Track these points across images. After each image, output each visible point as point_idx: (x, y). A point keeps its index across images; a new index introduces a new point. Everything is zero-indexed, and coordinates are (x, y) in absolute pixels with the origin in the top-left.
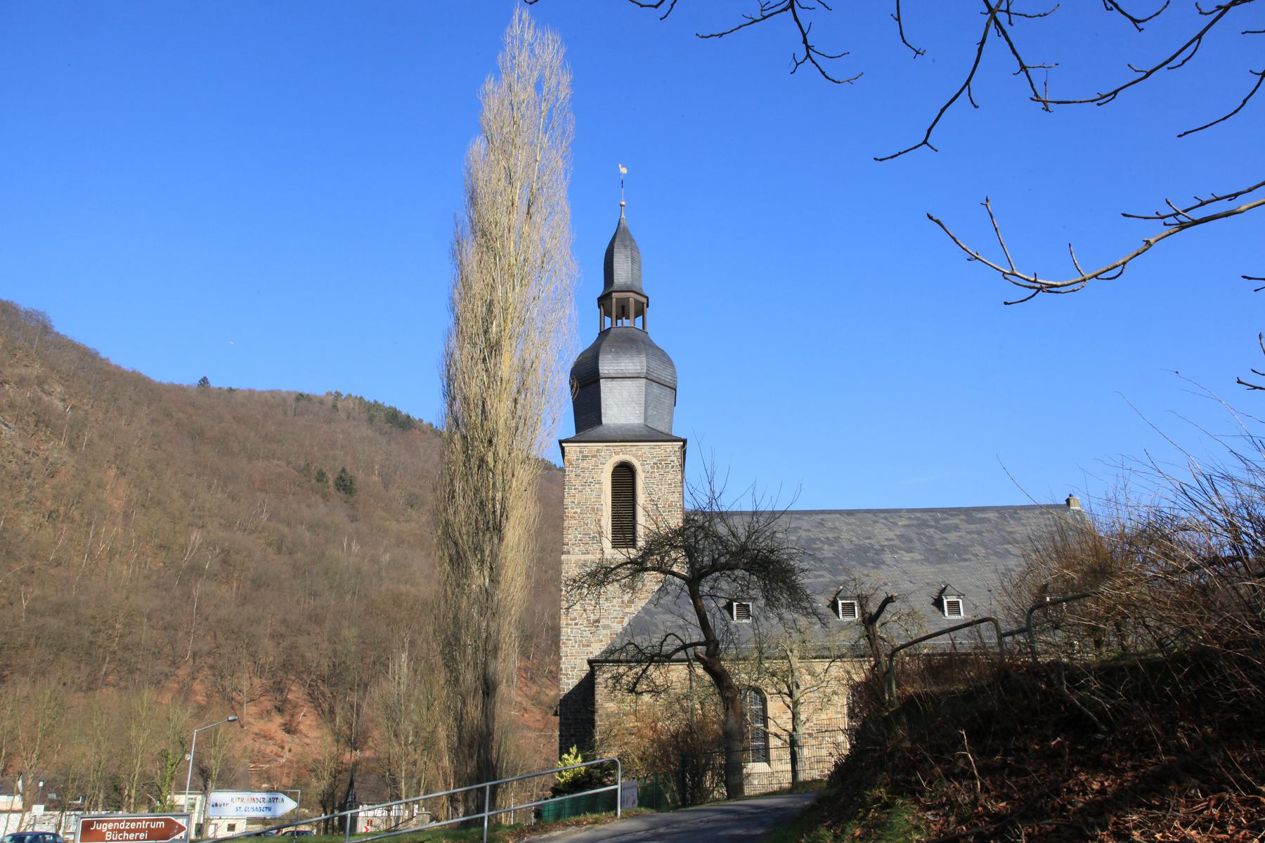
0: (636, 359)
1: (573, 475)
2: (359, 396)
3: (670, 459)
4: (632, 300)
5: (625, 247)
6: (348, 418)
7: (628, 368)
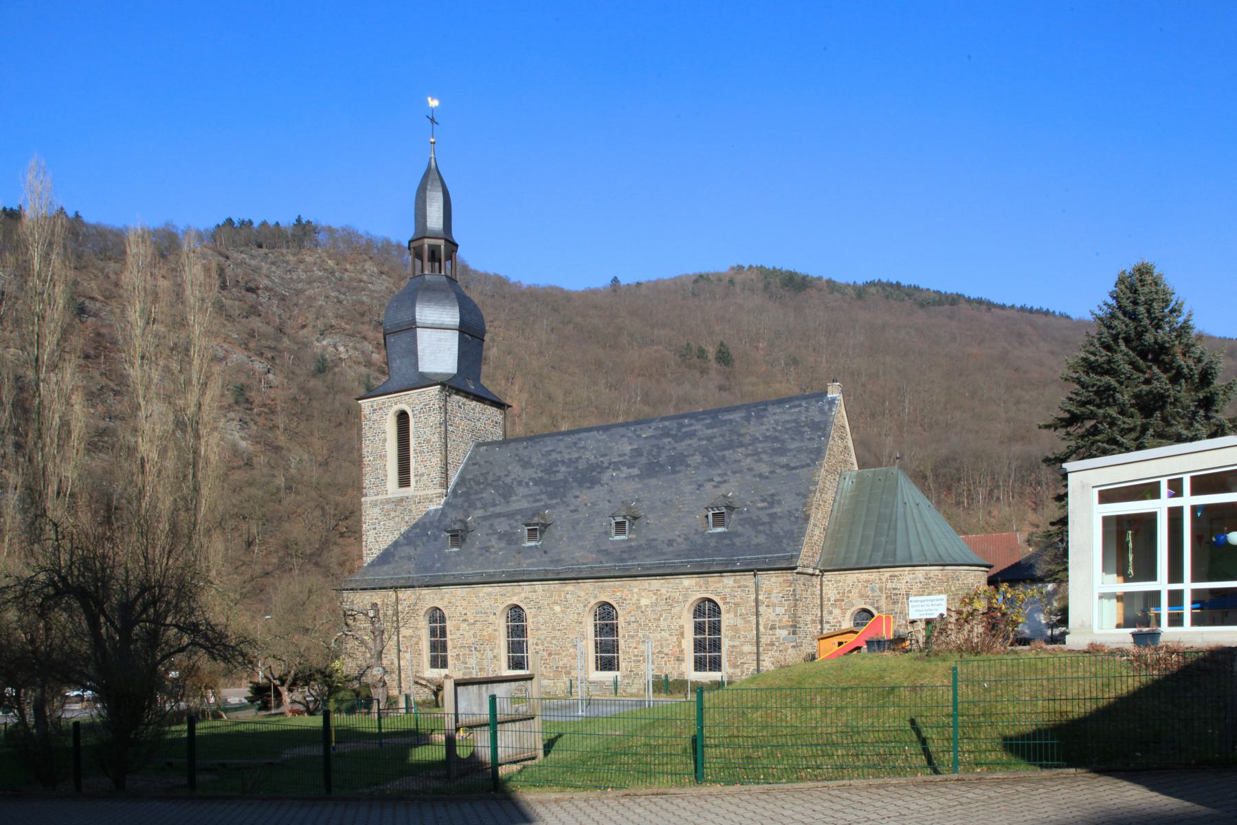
1: (367, 428)
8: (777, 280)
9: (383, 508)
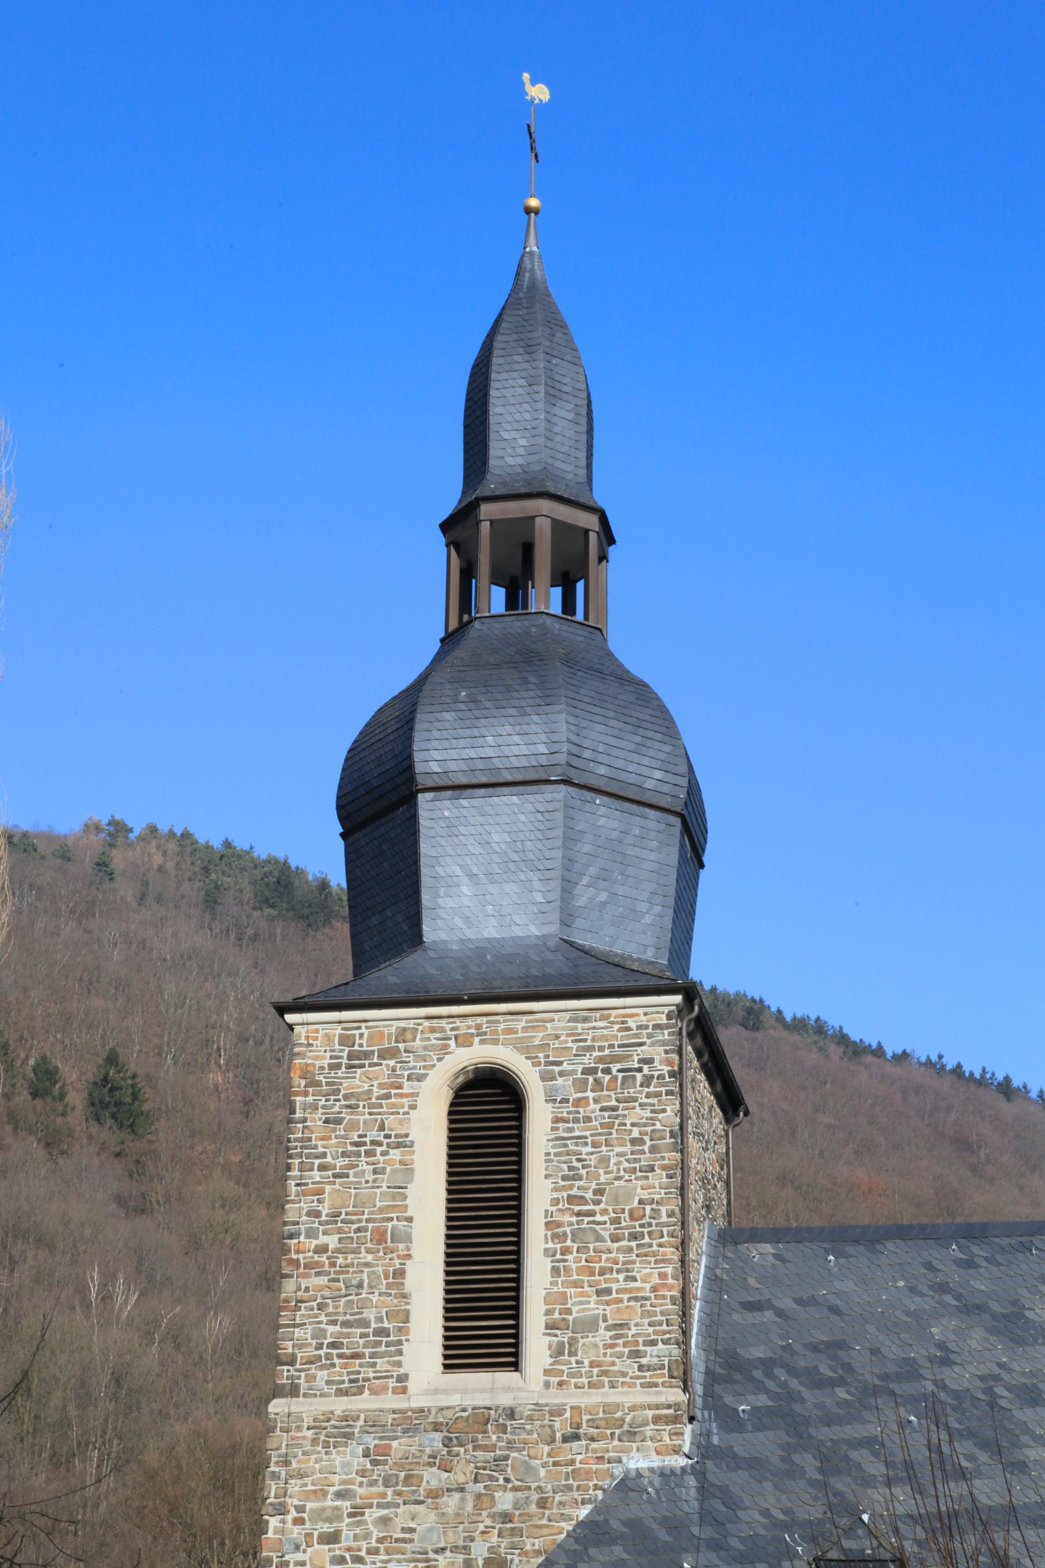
0: (536, 724)
1: (316, 1120)
2: (178, 832)
3: (644, 1051)
4: (543, 528)
5: (529, 349)
6: (142, 898)
7: (507, 751)
8: (245, 882)
9: (385, 1451)
